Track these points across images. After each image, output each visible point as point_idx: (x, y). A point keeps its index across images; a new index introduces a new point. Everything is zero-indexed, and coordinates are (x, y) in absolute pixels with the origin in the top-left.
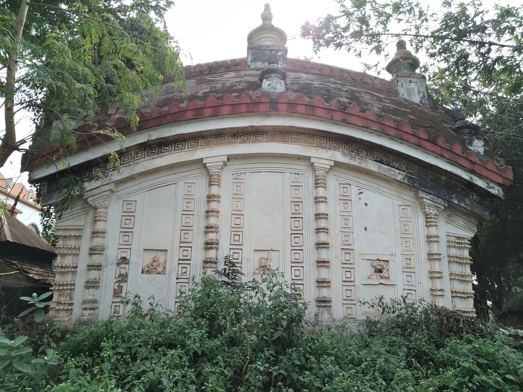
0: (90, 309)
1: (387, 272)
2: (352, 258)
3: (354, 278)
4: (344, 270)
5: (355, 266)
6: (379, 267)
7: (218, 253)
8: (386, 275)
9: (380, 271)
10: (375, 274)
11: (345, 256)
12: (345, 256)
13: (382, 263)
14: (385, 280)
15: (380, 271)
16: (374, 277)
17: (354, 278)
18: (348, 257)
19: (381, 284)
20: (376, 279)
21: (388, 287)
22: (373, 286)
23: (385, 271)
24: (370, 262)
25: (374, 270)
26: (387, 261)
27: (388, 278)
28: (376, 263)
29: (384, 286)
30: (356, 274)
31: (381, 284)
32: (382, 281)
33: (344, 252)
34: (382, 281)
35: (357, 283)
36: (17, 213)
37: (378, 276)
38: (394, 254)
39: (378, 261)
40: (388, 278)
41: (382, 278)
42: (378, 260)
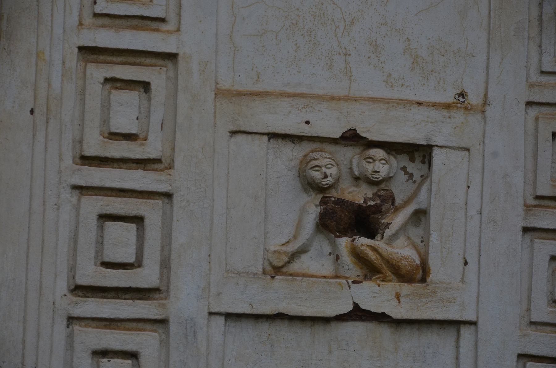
0: (541, 16)
1: (415, 233)
2: (156, 117)
3: (165, 264)
4: (95, 205)
5: (178, 180)
6: (359, 195)
7: (479, 336)
8: (403, 251)
9: (364, 221)
10: (322, 245)
11: (106, 107)
12: (106, 107)
13: (381, 165)
14: (392, 287)
15: (364, 221)
16: (316, 262)
17: (165, 264)
18: (125, 111)
19: (358, 314)
20: (325, 281)
21: (410, 340)
22: (304, 334)
23: (398, 220)
24: (292, 154)
25: (313, 213)
26: (419, 153)
27: (416, 275)
28: (331, 166)
29: (384, 332)
30: (179, 238)
31: (358, 314)
32: (375, 296)
33: (98, 72)
34: (375, 296)
35: (185, 301)
36: (226, 320)
37: (347, 259)
38: (474, 99)
39: (348, 154)
40: (416, 275)
41: (370, 269)
42: (351, 138)
